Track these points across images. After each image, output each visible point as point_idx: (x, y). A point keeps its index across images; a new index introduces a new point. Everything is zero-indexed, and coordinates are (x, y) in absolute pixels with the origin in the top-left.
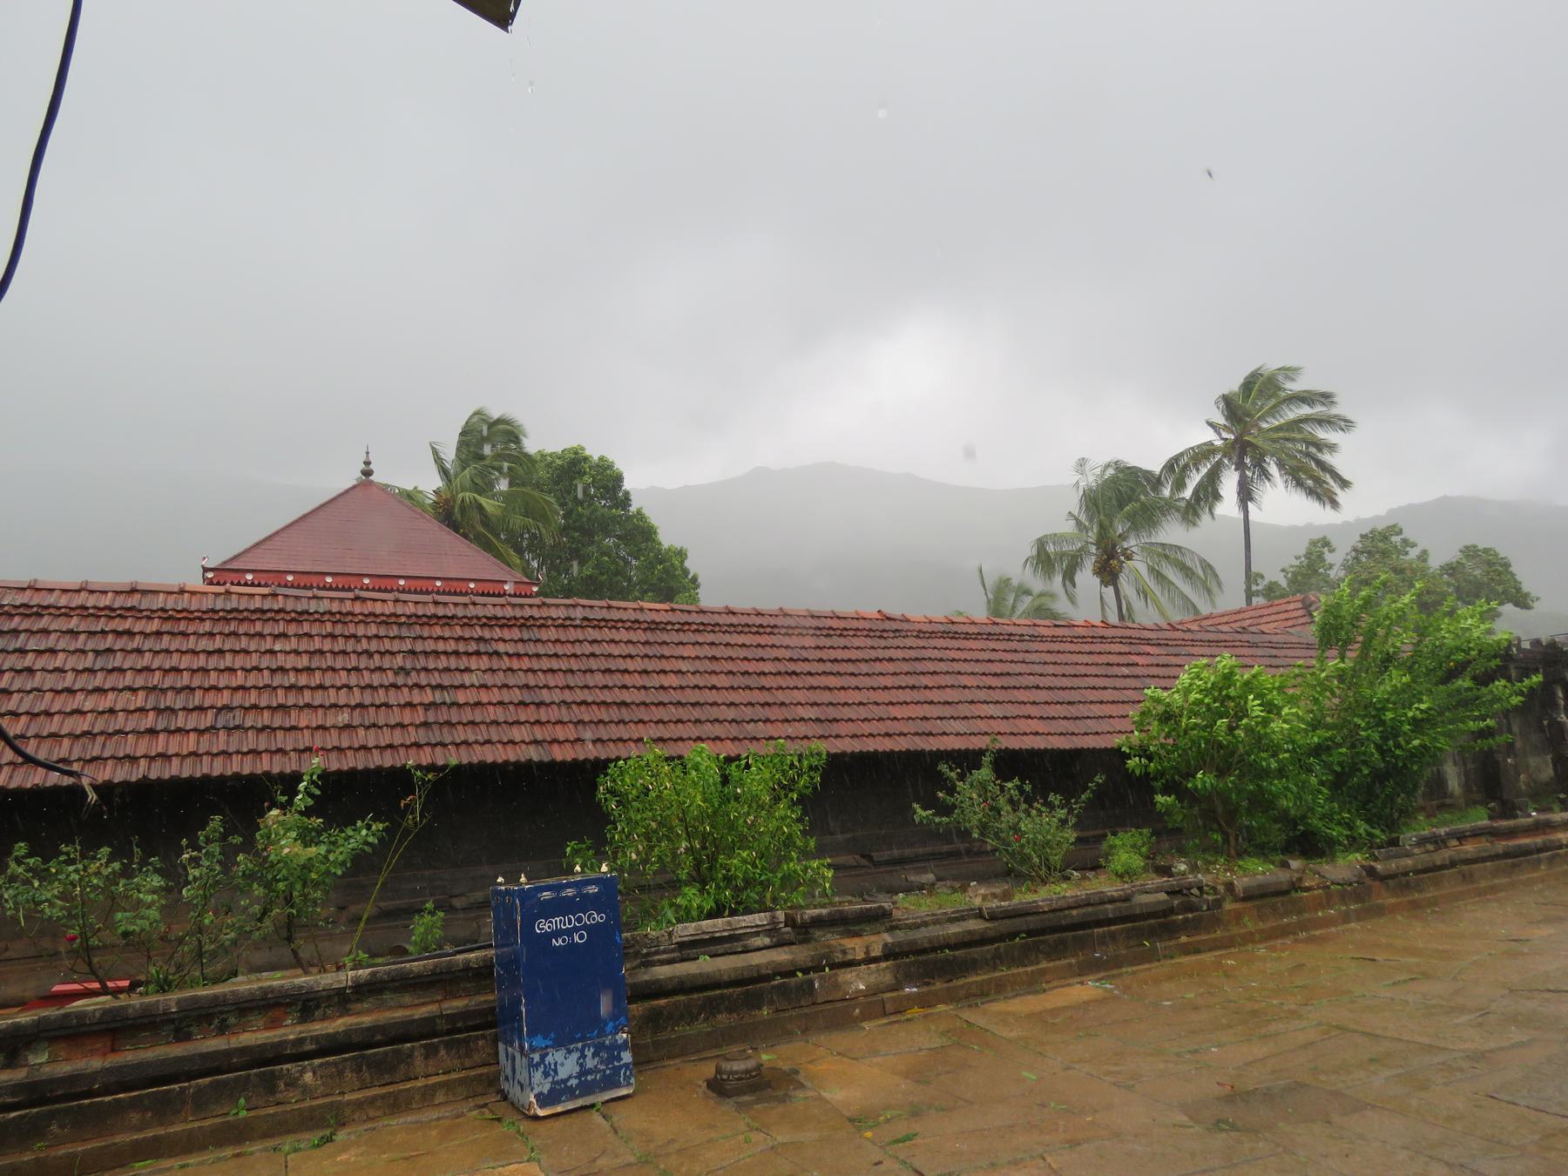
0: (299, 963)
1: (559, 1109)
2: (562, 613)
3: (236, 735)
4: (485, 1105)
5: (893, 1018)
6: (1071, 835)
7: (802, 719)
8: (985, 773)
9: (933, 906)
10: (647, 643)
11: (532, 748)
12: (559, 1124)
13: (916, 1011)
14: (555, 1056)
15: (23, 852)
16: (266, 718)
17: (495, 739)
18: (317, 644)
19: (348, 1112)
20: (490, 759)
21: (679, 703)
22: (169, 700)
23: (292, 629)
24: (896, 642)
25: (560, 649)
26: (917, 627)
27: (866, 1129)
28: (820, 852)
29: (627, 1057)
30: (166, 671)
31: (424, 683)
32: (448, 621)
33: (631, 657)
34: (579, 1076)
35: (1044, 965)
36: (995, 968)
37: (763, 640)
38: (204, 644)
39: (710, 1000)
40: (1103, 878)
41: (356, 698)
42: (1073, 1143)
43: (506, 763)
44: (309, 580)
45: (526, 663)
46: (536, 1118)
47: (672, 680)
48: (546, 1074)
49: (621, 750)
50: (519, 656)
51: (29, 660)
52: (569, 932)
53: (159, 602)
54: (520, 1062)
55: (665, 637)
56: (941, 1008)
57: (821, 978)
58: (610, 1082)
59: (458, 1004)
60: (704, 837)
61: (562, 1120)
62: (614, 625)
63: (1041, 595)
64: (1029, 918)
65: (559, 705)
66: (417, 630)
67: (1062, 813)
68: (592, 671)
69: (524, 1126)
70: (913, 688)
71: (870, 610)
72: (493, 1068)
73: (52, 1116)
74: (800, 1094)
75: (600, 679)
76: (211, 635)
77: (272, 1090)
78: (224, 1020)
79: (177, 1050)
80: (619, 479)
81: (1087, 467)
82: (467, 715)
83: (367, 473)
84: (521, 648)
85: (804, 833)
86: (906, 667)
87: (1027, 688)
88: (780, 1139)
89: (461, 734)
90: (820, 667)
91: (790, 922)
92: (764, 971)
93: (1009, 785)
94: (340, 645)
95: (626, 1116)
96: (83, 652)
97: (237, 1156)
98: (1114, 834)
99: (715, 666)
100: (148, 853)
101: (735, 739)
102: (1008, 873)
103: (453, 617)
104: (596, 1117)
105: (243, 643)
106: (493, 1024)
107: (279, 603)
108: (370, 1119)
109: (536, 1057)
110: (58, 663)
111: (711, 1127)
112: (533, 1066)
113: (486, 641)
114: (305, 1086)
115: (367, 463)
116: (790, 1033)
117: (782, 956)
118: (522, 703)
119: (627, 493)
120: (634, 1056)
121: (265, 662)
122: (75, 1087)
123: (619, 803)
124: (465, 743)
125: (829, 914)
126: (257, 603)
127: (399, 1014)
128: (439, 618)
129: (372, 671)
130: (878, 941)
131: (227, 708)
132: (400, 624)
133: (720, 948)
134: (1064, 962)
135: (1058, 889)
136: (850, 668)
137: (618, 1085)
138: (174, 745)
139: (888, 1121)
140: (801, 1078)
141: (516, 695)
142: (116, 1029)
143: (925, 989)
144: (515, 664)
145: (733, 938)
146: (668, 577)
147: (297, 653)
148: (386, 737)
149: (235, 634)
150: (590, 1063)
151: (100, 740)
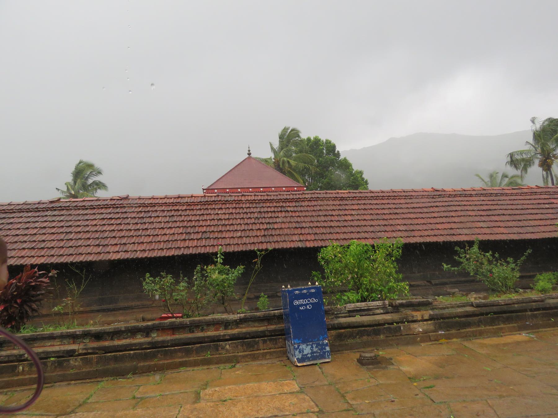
0: (226, 311)
1: (305, 364)
2: (309, 196)
3: (208, 240)
4: (282, 361)
5: (433, 342)
6: (518, 275)
7: (399, 230)
8: (475, 248)
9: (453, 301)
10: (340, 205)
11: (299, 243)
12: (303, 369)
13: (443, 341)
14: (303, 346)
15: (148, 276)
16: (216, 235)
17: (287, 240)
18: (231, 211)
19: (240, 358)
20: (285, 247)
21: (352, 226)
22: (189, 230)
23: (223, 206)
24: (439, 200)
25: (309, 209)
26: (449, 193)
27: (415, 382)
28: (403, 280)
29: (328, 349)
30: (196, 221)
31: (264, 222)
32: (271, 201)
33: (334, 210)
34: (311, 353)
35: (502, 326)
36: (479, 326)
37: (408, 201)
38: (199, 212)
39: (361, 331)
40: (534, 292)
41: (243, 227)
42: (501, 397)
43: (290, 248)
44: (233, 190)
45: (297, 214)
46: (297, 366)
47: (349, 218)
48: (300, 352)
49: (327, 243)
50: (295, 212)
51: (152, 220)
52: (306, 305)
53: (186, 200)
54: (292, 348)
55: (347, 202)
56: (455, 340)
57: (404, 326)
58: (323, 357)
59: (272, 327)
60: (357, 273)
61: (306, 367)
62: (328, 199)
63: (513, 177)
64: (494, 307)
65: (308, 228)
66: (261, 205)
67: (513, 266)
68: (320, 216)
69: (293, 368)
70: (446, 217)
71: (428, 188)
72: (284, 349)
73: (158, 352)
74: (391, 367)
75: (323, 219)
76: (200, 209)
77: (217, 350)
78: (203, 328)
79: (190, 335)
80: (334, 147)
81: (536, 121)
82: (278, 232)
83: (249, 154)
84: (296, 209)
85: (396, 272)
86: (443, 209)
87: (499, 215)
88: (381, 382)
89: (275, 239)
90: (407, 211)
91: (391, 305)
92: (381, 322)
93: (487, 254)
94: (238, 211)
95: (328, 369)
96: (166, 216)
97: (208, 369)
98: (540, 274)
99: (366, 212)
100: (184, 276)
101: (373, 238)
102: (486, 290)
103: (273, 200)
104: (317, 368)
105: (210, 211)
106: (283, 333)
107: (220, 198)
108: (246, 362)
109: (296, 346)
110: (160, 220)
111: (356, 375)
112: (295, 349)
113: (284, 207)
114: (227, 349)
115: (249, 151)
116: (392, 345)
117: (388, 317)
118: (296, 228)
119: (338, 152)
120: (330, 348)
121: (216, 217)
122: (162, 345)
123: (325, 262)
124: (277, 241)
125: (407, 302)
126: (213, 199)
127: (254, 329)
128: (269, 200)
129: (248, 219)
130: (427, 314)
131: (205, 232)
132: (256, 203)
133: (364, 313)
134: (511, 325)
135: (510, 296)
136: (420, 210)
137: (325, 358)
138: (190, 244)
139: (424, 380)
140: (393, 361)
141: (294, 225)
142: (174, 328)
143: (447, 332)
144: (294, 214)
145: (368, 310)
146: (356, 181)
147: (225, 214)
148: (252, 240)
149: (207, 209)
150: (315, 349)
151: (171, 242)
